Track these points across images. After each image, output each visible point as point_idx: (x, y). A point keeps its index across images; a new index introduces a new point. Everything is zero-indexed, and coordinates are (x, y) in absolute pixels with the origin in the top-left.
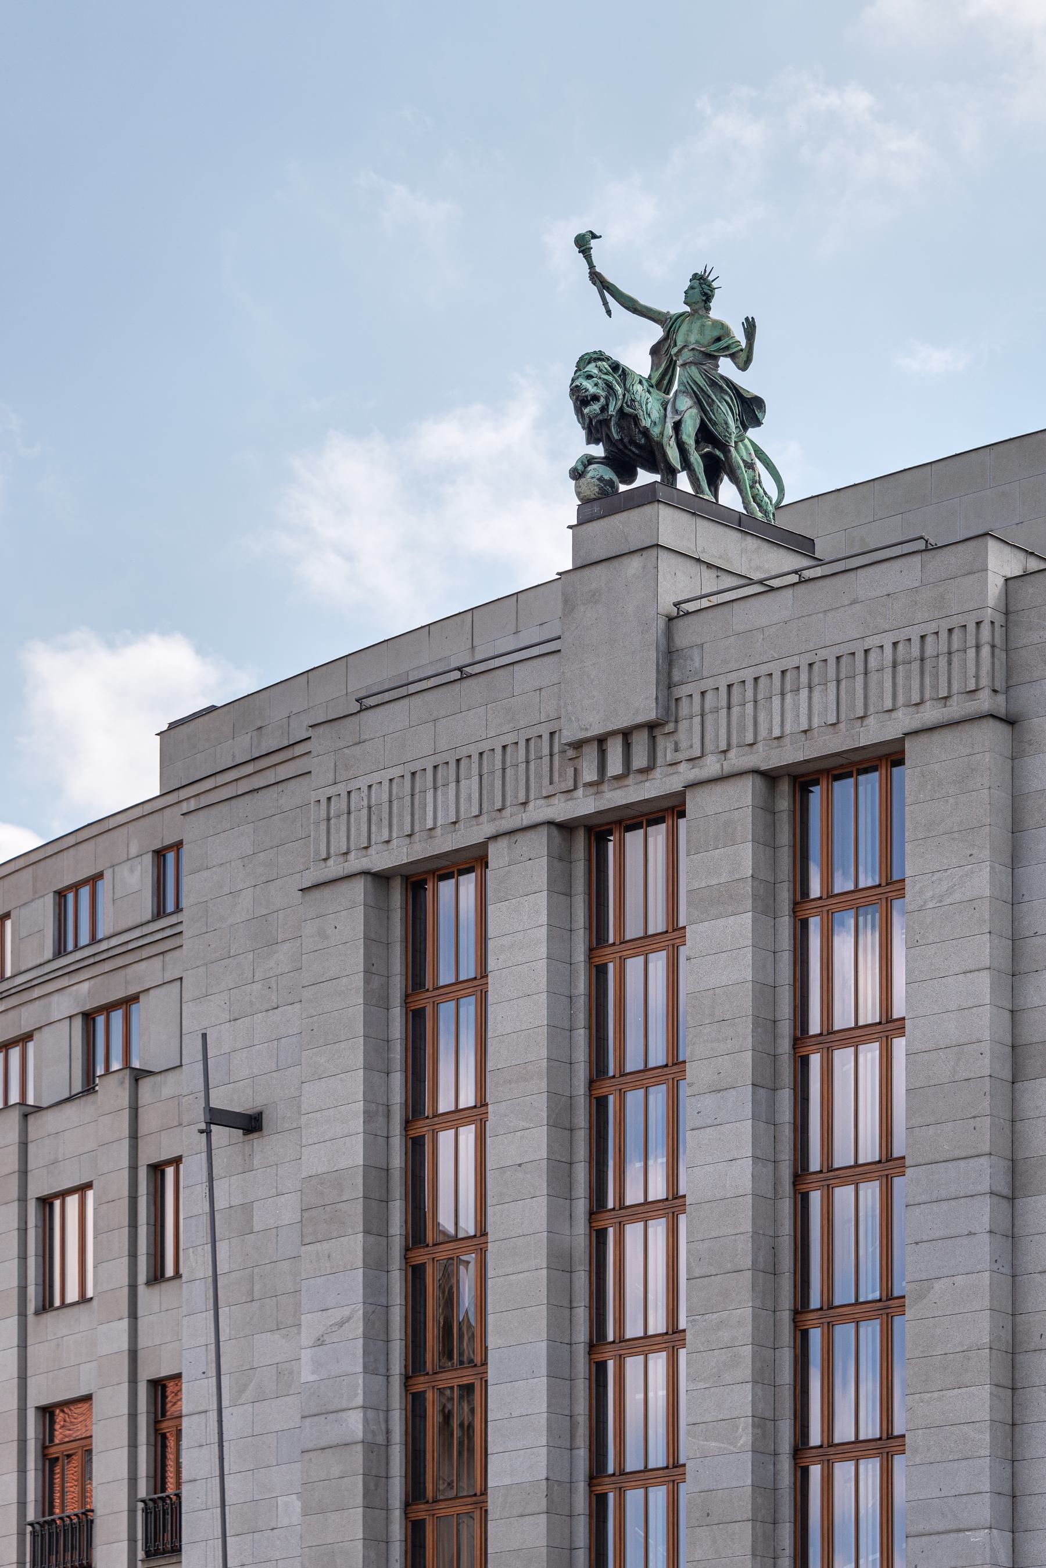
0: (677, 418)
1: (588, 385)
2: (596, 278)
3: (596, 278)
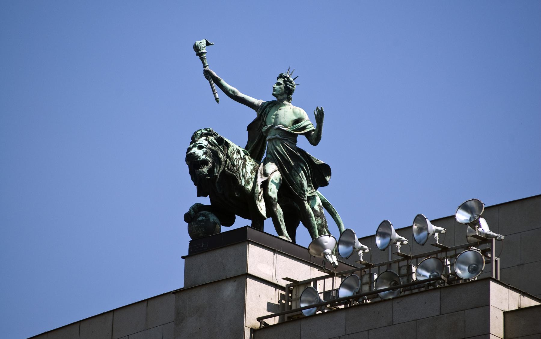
0: (265, 179)
1: (200, 153)
2: (208, 75)
3: (208, 75)
